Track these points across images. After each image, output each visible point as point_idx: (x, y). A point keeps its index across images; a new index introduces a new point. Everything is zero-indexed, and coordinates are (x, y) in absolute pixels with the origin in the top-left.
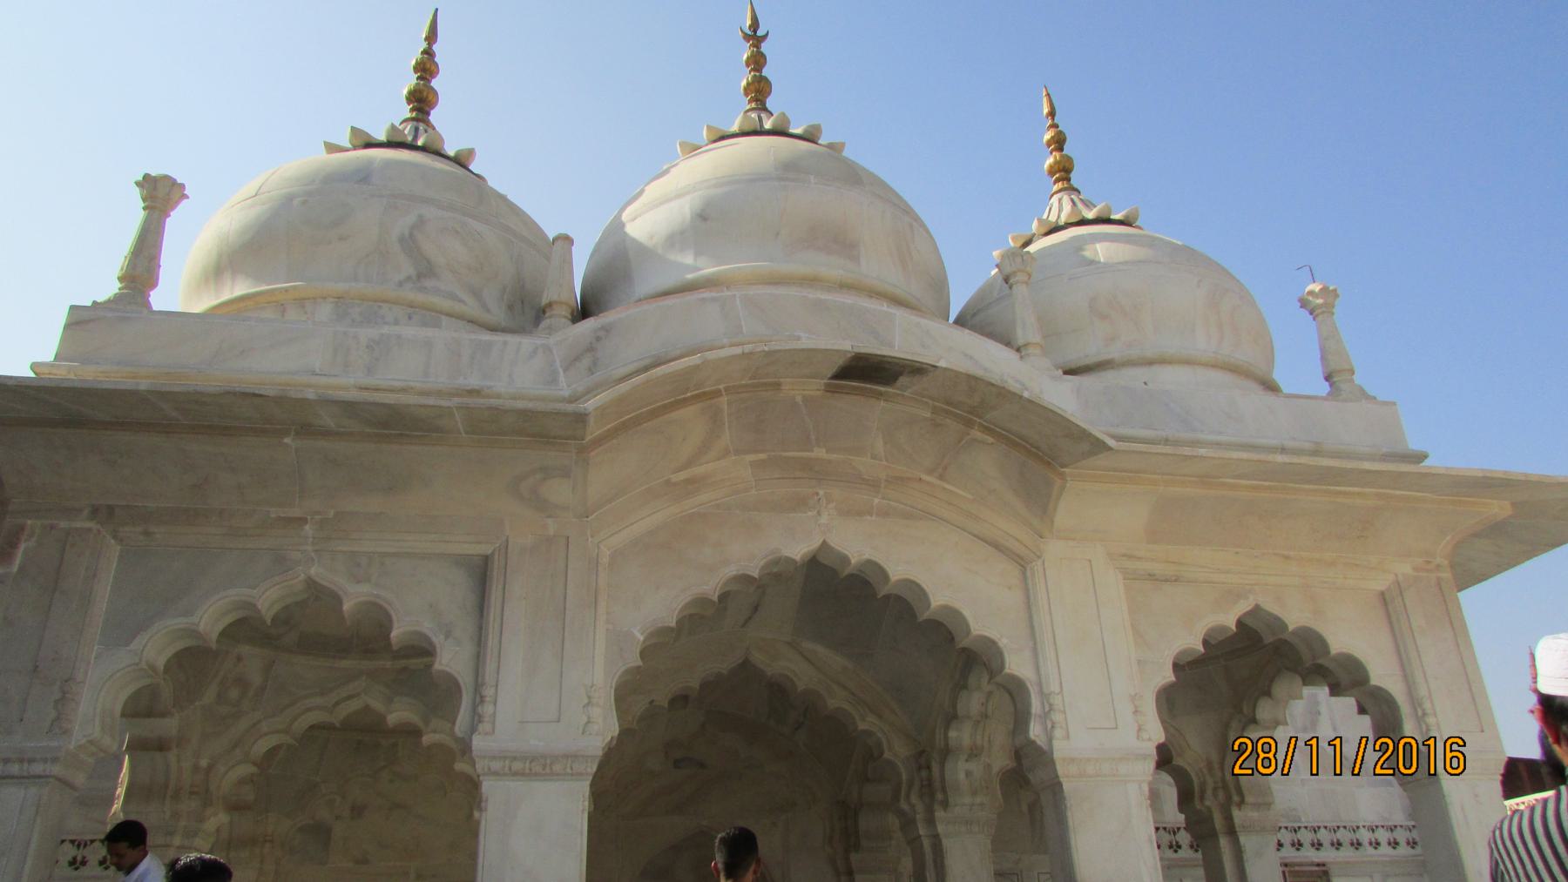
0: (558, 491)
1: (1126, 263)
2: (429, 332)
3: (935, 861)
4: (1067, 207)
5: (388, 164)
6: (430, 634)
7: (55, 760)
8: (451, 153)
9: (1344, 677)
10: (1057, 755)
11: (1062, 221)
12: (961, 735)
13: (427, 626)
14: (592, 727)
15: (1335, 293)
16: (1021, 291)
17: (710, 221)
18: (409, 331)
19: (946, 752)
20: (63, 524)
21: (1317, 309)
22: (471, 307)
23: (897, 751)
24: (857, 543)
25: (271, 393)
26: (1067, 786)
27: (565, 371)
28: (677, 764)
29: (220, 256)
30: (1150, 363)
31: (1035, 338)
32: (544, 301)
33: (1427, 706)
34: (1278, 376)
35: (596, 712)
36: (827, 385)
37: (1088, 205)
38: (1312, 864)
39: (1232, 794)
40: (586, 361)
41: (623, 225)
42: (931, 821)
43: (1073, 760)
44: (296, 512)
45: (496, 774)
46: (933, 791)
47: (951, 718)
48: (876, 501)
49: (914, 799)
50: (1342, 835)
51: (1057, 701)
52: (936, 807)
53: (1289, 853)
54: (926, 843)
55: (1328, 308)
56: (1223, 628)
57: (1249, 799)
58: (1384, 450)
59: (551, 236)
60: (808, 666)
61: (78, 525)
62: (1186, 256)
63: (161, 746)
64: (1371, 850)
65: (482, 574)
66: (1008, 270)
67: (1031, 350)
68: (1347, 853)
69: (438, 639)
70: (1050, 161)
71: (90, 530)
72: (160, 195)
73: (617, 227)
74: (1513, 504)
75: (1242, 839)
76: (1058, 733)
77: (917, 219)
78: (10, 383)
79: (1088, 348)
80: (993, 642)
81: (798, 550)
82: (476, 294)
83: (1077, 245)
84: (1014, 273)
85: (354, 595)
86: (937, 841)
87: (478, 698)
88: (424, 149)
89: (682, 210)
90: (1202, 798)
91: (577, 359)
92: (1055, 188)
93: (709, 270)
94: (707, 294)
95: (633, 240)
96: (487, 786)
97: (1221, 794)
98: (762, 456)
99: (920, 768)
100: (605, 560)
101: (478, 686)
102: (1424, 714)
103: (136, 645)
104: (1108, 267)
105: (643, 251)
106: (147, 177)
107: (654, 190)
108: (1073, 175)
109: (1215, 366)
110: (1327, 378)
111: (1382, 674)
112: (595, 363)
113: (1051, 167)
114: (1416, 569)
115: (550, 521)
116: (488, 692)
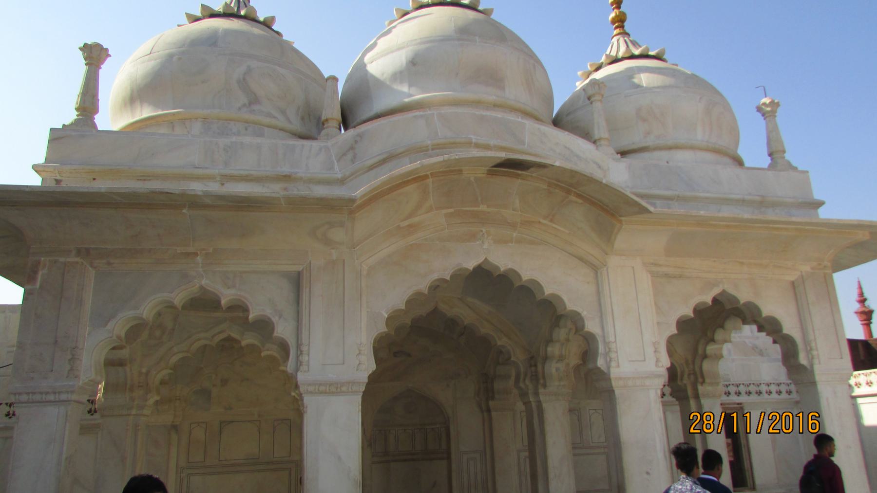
0: (337, 235)
1: (658, 87)
2: (259, 140)
3: (539, 415)
4: (623, 49)
5: (227, 32)
6: (271, 317)
7: (72, 392)
8: (262, 19)
9: (771, 327)
10: (612, 376)
11: (620, 55)
12: (554, 350)
13: (268, 312)
14: (362, 366)
15: (778, 104)
16: (597, 106)
17: (417, 66)
18: (247, 140)
19: (546, 358)
20: (62, 260)
21: (768, 113)
22: (281, 122)
23: (519, 356)
24: (503, 259)
25: (177, 192)
26: (617, 392)
27: (338, 161)
28: (395, 354)
29: (132, 91)
30: (670, 148)
31: (606, 136)
32: (323, 118)
33: (813, 345)
34: (742, 152)
35: (363, 358)
36: (489, 170)
37: (635, 44)
38: (735, 404)
39: (699, 377)
40: (350, 156)
41: (365, 65)
42: (536, 394)
43: (620, 378)
44: (191, 249)
45: (311, 393)
46: (538, 378)
47: (549, 341)
48: (515, 234)
49: (528, 382)
50: (752, 388)
51: (613, 346)
52: (540, 387)
53: (725, 398)
54: (533, 404)
55: (773, 114)
56: (704, 303)
57: (707, 380)
58: (800, 200)
59: (326, 76)
60: (467, 312)
61: (69, 260)
62: (694, 83)
63: (121, 363)
64: (766, 396)
65: (297, 282)
66: (590, 92)
67: (603, 142)
68: (754, 398)
69: (275, 319)
70: (613, 15)
71: (77, 263)
72: (95, 55)
73: (360, 67)
74: (871, 233)
75: (702, 401)
76: (613, 364)
77: (538, 61)
78: (27, 190)
79: (634, 138)
80: (579, 314)
81: (471, 264)
82: (283, 112)
83: (630, 74)
84: (594, 95)
85: (227, 296)
86: (539, 403)
87: (299, 352)
88: (245, 17)
89: (400, 59)
90: (682, 379)
91: (344, 154)
92: (616, 32)
93: (419, 97)
94: (417, 113)
95: (372, 76)
96: (307, 399)
97: (692, 377)
98: (452, 210)
99: (531, 366)
100: (365, 273)
101: (299, 346)
102: (811, 349)
103: (110, 326)
104: (649, 90)
105: (377, 81)
106: (86, 45)
107: (383, 44)
108: (625, 24)
109: (707, 150)
110: (770, 155)
111: (790, 327)
112: (355, 157)
113: (613, 19)
114: (812, 268)
115: (333, 251)
116: (305, 349)
